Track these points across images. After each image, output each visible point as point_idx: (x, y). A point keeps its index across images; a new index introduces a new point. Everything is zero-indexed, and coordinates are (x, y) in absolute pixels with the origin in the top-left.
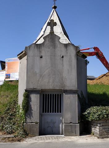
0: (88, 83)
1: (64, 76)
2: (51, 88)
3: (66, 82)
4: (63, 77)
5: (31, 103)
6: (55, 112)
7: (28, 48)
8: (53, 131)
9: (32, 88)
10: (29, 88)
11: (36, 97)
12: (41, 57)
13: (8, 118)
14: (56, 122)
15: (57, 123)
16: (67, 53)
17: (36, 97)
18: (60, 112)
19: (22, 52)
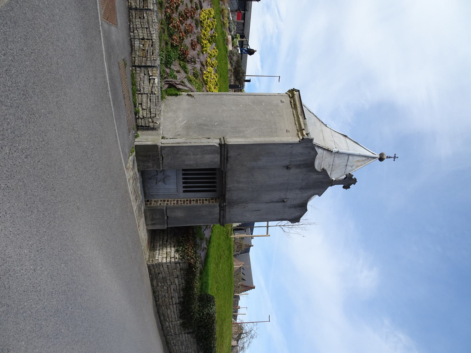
0: (131, 35)
1: (249, 204)
2: (228, 186)
3: (237, 208)
4: (248, 203)
5: (175, 96)
6: (184, 183)
7: (310, 145)
8: (150, 179)
9: (229, 155)
10: (229, 149)
11: (211, 162)
12: (288, 168)
13: (234, 238)
14: (166, 184)
15: (165, 185)
16: (290, 208)
17: (211, 162)
18: (184, 191)
19: (291, 102)
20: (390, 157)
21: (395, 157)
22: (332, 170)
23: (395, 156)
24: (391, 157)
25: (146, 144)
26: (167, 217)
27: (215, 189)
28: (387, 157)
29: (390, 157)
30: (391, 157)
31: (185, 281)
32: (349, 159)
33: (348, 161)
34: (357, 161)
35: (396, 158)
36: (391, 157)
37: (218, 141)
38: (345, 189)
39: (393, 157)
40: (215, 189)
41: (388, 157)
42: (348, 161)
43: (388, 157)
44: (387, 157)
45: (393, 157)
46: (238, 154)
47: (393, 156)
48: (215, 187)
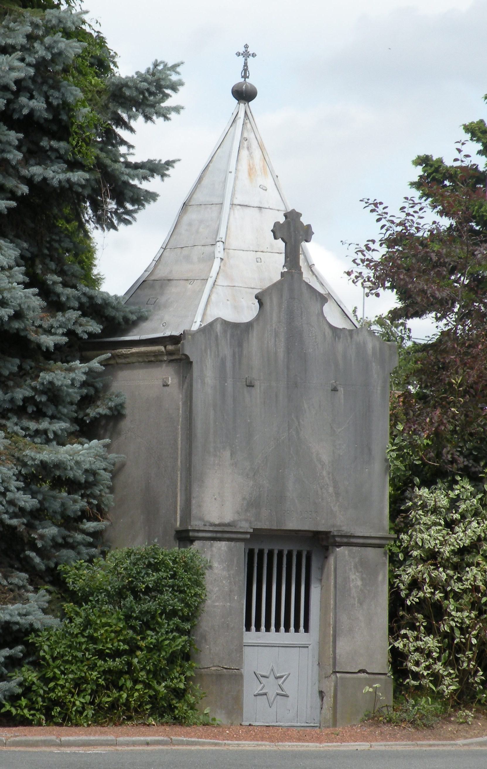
9: (217, 522)
20: (246, 69)
21: (246, 54)
22: (269, 250)
23: (242, 54)
24: (246, 65)
25: (154, 346)
26: (361, 671)
27: (276, 552)
28: (245, 77)
29: (246, 69)
30: (246, 65)
31: (55, 489)
32: (242, 204)
33: (249, 206)
34: (250, 175)
35: (251, 57)
36: (244, 66)
37: (57, 363)
38: (313, 236)
39: (246, 60)
40: (276, 552)
41: (245, 73)
42: (249, 206)
43: (245, 73)
44: (245, 77)
45: (246, 60)
46: (214, 500)
47: (241, 59)
48: (290, 554)
